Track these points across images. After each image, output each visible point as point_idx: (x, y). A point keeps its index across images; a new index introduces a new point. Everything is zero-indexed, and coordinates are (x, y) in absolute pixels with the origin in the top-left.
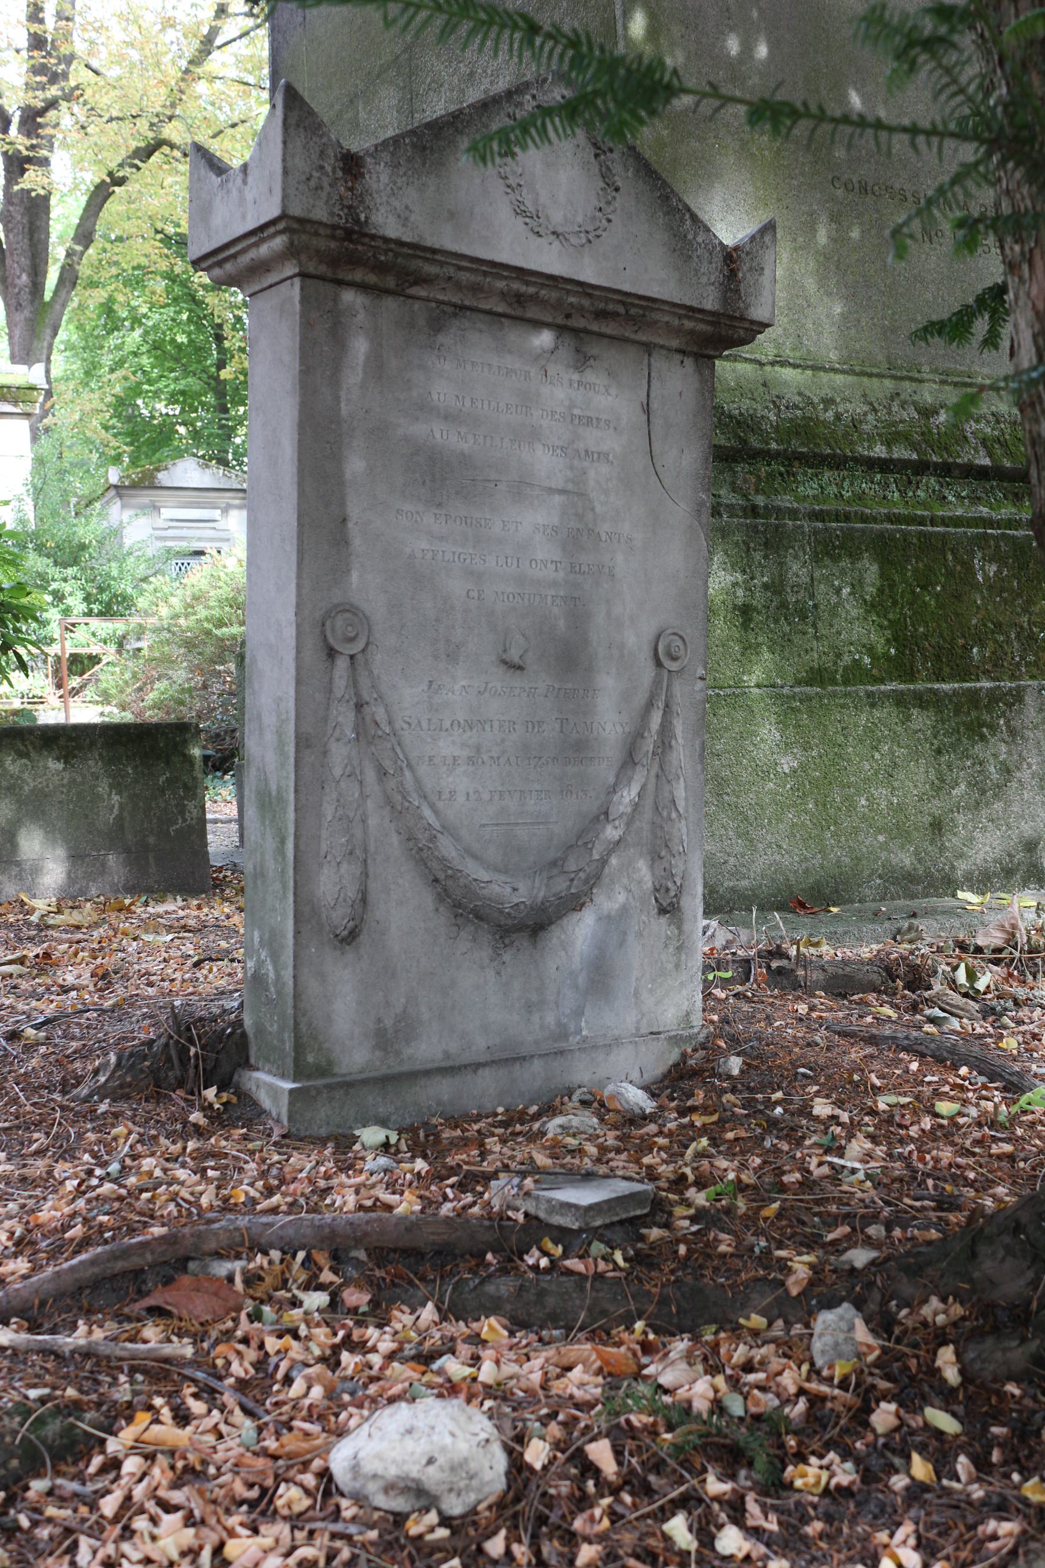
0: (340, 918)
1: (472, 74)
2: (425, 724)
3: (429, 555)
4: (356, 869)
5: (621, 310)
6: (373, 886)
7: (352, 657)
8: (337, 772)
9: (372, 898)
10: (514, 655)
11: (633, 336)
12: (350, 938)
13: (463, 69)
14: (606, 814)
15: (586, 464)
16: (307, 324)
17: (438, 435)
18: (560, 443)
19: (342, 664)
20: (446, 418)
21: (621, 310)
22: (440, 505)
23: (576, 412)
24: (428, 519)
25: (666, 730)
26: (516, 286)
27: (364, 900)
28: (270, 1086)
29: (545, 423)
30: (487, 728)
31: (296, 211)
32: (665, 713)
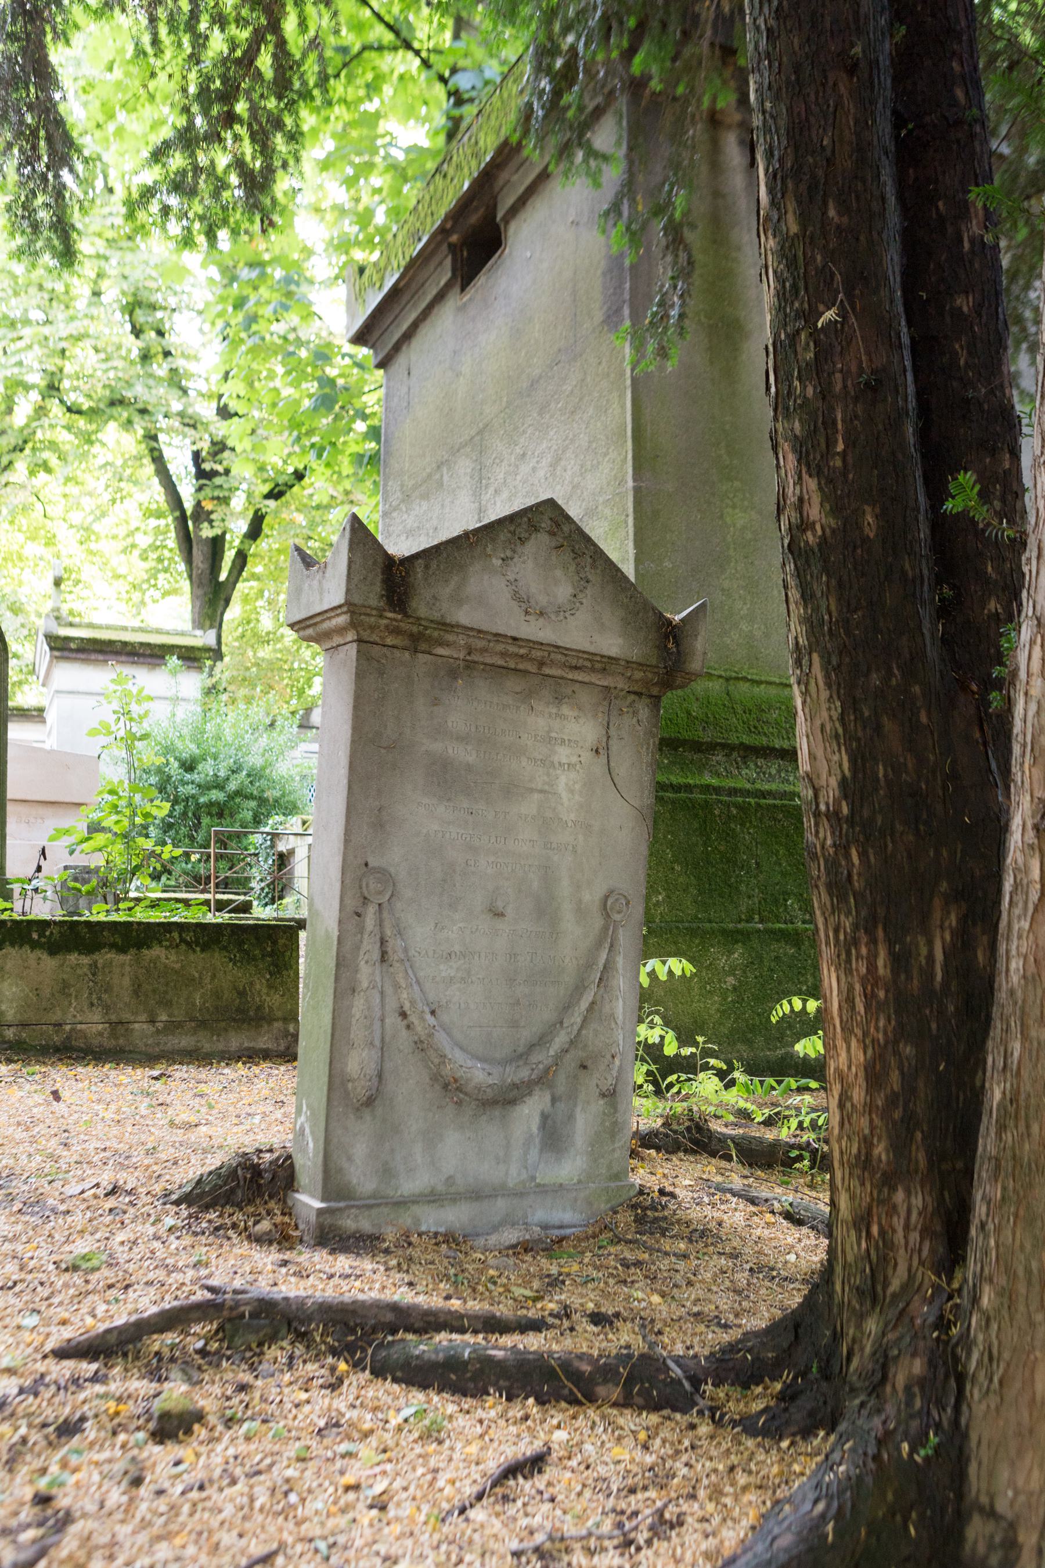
0: (360, 1089)
1: (524, 455)
4: (375, 1054)
5: (588, 664)
6: (388, 1066)
8: (365, 985)
10: (500, 904)
12: (370, 1102)
13: (518, 450)
16: (360, 676)
21: (588, 664)
24: (441, 809)
26: (512, 649)
27: (380, 1076)
28: (309, 1201)
31: (357, 599)
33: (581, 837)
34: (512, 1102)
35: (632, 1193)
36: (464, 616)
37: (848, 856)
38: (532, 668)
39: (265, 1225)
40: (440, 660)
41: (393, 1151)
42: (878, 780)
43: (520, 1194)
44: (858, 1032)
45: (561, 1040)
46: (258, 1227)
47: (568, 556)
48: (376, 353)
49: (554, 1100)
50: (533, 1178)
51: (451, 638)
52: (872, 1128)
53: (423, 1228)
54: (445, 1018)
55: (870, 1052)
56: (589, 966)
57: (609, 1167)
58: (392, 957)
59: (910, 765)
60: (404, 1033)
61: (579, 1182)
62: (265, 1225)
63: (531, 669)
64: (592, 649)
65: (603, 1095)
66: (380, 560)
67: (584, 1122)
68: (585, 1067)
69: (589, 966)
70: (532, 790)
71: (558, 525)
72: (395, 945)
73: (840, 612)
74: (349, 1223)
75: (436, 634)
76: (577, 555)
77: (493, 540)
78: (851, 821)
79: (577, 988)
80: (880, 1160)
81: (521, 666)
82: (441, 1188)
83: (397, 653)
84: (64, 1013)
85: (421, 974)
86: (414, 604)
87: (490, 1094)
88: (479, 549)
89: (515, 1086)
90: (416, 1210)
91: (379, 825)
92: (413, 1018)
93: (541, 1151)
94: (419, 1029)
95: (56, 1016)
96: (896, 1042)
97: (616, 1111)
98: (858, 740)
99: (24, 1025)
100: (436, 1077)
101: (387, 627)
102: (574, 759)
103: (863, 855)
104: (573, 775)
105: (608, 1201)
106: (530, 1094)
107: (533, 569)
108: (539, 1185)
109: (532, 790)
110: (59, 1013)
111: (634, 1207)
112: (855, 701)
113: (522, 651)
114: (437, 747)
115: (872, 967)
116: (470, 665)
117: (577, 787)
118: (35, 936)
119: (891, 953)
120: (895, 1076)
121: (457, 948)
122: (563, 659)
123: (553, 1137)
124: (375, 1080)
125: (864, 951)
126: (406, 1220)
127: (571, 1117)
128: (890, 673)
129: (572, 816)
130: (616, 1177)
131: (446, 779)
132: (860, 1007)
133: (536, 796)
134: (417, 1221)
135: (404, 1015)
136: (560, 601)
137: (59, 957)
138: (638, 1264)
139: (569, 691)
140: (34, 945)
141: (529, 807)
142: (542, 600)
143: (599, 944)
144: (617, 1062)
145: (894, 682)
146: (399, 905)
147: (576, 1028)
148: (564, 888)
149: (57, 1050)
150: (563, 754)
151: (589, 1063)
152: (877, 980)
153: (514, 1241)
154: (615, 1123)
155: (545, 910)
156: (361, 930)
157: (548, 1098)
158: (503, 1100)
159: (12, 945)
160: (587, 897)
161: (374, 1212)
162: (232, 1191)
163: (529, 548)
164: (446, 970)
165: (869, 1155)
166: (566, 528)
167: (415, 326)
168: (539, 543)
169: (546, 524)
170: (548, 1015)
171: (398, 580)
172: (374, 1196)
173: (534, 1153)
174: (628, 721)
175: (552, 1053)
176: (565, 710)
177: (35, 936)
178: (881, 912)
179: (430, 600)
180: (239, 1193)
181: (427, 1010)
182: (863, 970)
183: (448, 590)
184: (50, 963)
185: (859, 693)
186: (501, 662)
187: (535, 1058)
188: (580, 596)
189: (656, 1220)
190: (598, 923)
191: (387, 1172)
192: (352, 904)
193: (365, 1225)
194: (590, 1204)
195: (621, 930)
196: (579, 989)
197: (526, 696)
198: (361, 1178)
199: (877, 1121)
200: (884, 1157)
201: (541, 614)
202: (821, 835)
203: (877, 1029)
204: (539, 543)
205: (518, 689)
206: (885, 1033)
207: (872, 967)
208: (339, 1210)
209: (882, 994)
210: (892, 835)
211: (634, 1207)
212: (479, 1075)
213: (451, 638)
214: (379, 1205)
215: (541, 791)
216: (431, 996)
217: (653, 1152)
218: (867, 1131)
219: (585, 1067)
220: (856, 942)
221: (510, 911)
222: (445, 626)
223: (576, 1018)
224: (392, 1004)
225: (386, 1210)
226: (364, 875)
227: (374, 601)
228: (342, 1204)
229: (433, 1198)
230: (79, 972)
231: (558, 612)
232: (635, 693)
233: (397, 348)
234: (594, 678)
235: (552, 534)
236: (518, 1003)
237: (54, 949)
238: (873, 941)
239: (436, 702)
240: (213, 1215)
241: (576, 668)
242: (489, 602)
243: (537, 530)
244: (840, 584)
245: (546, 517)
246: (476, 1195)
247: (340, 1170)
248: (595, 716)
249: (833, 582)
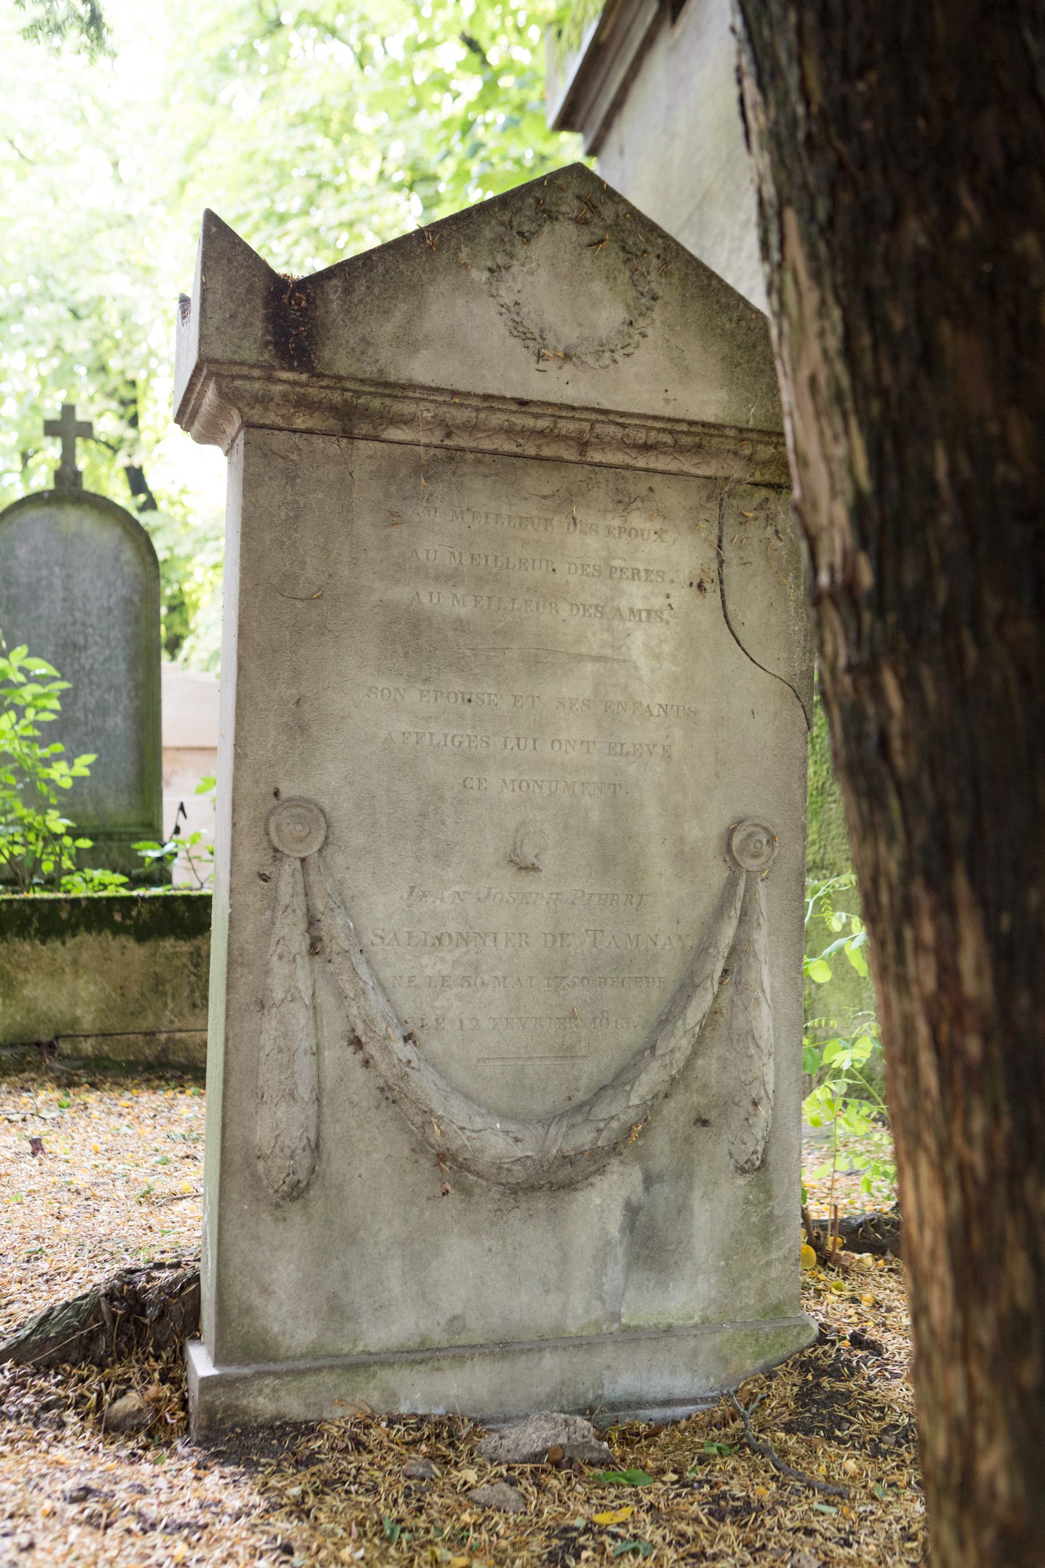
0: (277, 1172)
2: (403, 938)
3: (414, 738)
5: (668, 439)
6: (331, 1130)
7: (303, 860)
8: (278, 995)
9: (328, 1144)
10: (529, 853)
11: (693, 471)
12: (296, 1192)
14: (653, 1048)
15: (630, 625)
17: (425, 599)
18: (595, 601)
19: (290, 867)
20: (437, 578)
21: (668, 439)
22: (427, 680)
23: (617, 563)
25: (739, 952)
27: (316, 1148)
29: (573, 579)
30: (489, 942)
31: (217, 352)
32: (741, 921)
33: (678, 733)
34: (570, 1186)
35: (806, 1339)
36: (421, 369)
37: (877, 691)
38: (570, 454)
39: (132, 1401)
40: (398, 450)
41: (345, 1276)
42: (933, 488)
43: (584, 1344)
44: (929, 1140)
45: (651, 1078)
46: (119, 1404)
47: (612, 257)
48: (586, 137)
49: (649, 1181)
50: (616, 1317)
51: (407, 408)
52: (973, 1402)
53: (404, 1409)
54: (434, 1045)
55: (956, 1197)
56: (703, 950)
57: (762, 1293)
58: (331, 946)
59: (1017, 439)
60: (360, 1073)
61: (705, 1320)
62: (132, 1401)
63: (564, 451)
64: (668, 412)
65: (743, 1171)
66: (259, 284)
67: (710, 1215)
68: (705, 1123)
69: (703, 950)
70: (581, 658)
71: (593, 208)
72: (334, 925)
73: (826, 84)
74: (264, 1402)
75: (376, 403)
76: (630, 255)
77: (470, 239)
78: (879, 603)
79: (682, 987)
80: (993, 1494)
81: (546, 452)
82: (439, 1337)
83: (319, 443)
84: (158, 1018)
85: (386, 974)
86: (326, 354)
87: (519, 1174)
88: (445, 255)
89: (566, 1160)
90: (387, 1376)
91: (299, 726)
92: (372, 1049)
93: (629, 1267)
94: (383, 1067)
95: (147, 1022)
96: (1014, 1177)
97: (769, 1195)
98: (883, 393)
99: (105, 1035)
100: (421, 1147)
101: (284, 396)
102: (659, 602)
103: (909, 684)
104: (657, 629)
105: (759, 1355)
106: (601, 1171)
107: (551, 283)
108: (626, 1329)
109: (581, 658)
110: (151, 1017)
111: (804, 1366)
112: (869, 297)
113: (542, 424)
114: (401, 593)
115: (948, 973)
116: (452, 456)
117: (666, 648)
118: (118, 917)
119: (990, 933)
120: (1018, 1267)
121: (452, 927)
122: (619, 432)
123: (649, 1242)
124: (304, 1160)
125: (928, 933)
126: (370, 1394)
127: (683, 1209)
128: (950, 207)
129: (660, 698)
130: (776, 1311)
131: (415, 643)
132: (930, 1079)
133: (589, 667)
134: (392, 1397)
135: (357, 1043)
136: (603, 333)
137: (150, 945)
138: (745, 1511)
139: (642, 488)
140: (117, 930)
141: (577, 686)
142: (569, 334)
143: (720, 912)
144: (763, 1112)
145: (963, 231)
146: (340, 860)
147: (680, 1058)
148: (651, 818)
149: (149, 1067)
150: (636, 595)
151: (712, 1116)
152: (960, 1008)
153: (537, 1447)
154: (770, 1217)
155: (614, 856)
156: (272, 903)
157: (636, 1176)
158: (553, 1181)
159: (89, 930)
160: (693, 832)
161: (310, 1381)
162: (92, 1337)
163: (542, 246)
164: (432, 965)
165: (968, 1471)
166: (608, 212)
167: (625, 89)
168: (559, 239)
169: (569, 206)
170: (631, 1036)
171: (294, 315)
172: (312, 1353)
173: (615, 1273)
174: (757, 533)
175: (635, 1100)
176: (637, 520)
177: (118, 917)
178: (959, 827)
179: (361, 345)
180: (103, 1342)
181: (397, 1034)
182: (930, 982)
183: (389, 328)
184: (137, 952)
185: (878, 278)
186: (510, 447)
187: (602, 1111)
188: (641, 323)
189: (834, 1396)
190: (717, 875)
191: (337, 1311)
192: (253, 859)
193: (293, 1405)
194: (725, 1360)
195: (761, 887)
196: (686, 988)
197: (565, 501)
198: (287, 1317)
199: (982, 1385)
200: (1002, 1485)
201: (567, 357)
202: (829, 649)
203: (968, 1136)
204: (559, 239)
205: (547, 490)
206: (989, 1151)
207: (948, 973)
208: (244, 1379)
209: (973, 1046)
210: (975, 624)
211: (804, 1366)
212: (496, 1143)
213: (407, 408)
214: (317, 1370)
215: (599, 659)
216: (407, 1010)
217: (867, 1258)
218: (961, 1406)
219: (705, 1123)
220: (907, 911)
221: (549, 863)
222: (403, 389)
223: (680, 1041)
224: (333, 1027)
225: (328, 1379)
226: (272, 812)
227: (250, 352)
228: (246, 1371)
229: (421, 1355)
230: (177, 963)
231: (599, 354)
232: (768, 485)
233: (607, 124)
234: (686, 464)
235: (581, 222)
236: (573, 1016)
237: (143, 933)
238: (947, 907)
239: (394, 519)
240: (48, 1384)
241: (646, 448)
242: (466, 343)
243: (552, 217)
244: (825, 20)
245: (569, 195)
246: (504, 1348)
247: (248, 1310)
248: (694, 527)
249: (811, 19)
